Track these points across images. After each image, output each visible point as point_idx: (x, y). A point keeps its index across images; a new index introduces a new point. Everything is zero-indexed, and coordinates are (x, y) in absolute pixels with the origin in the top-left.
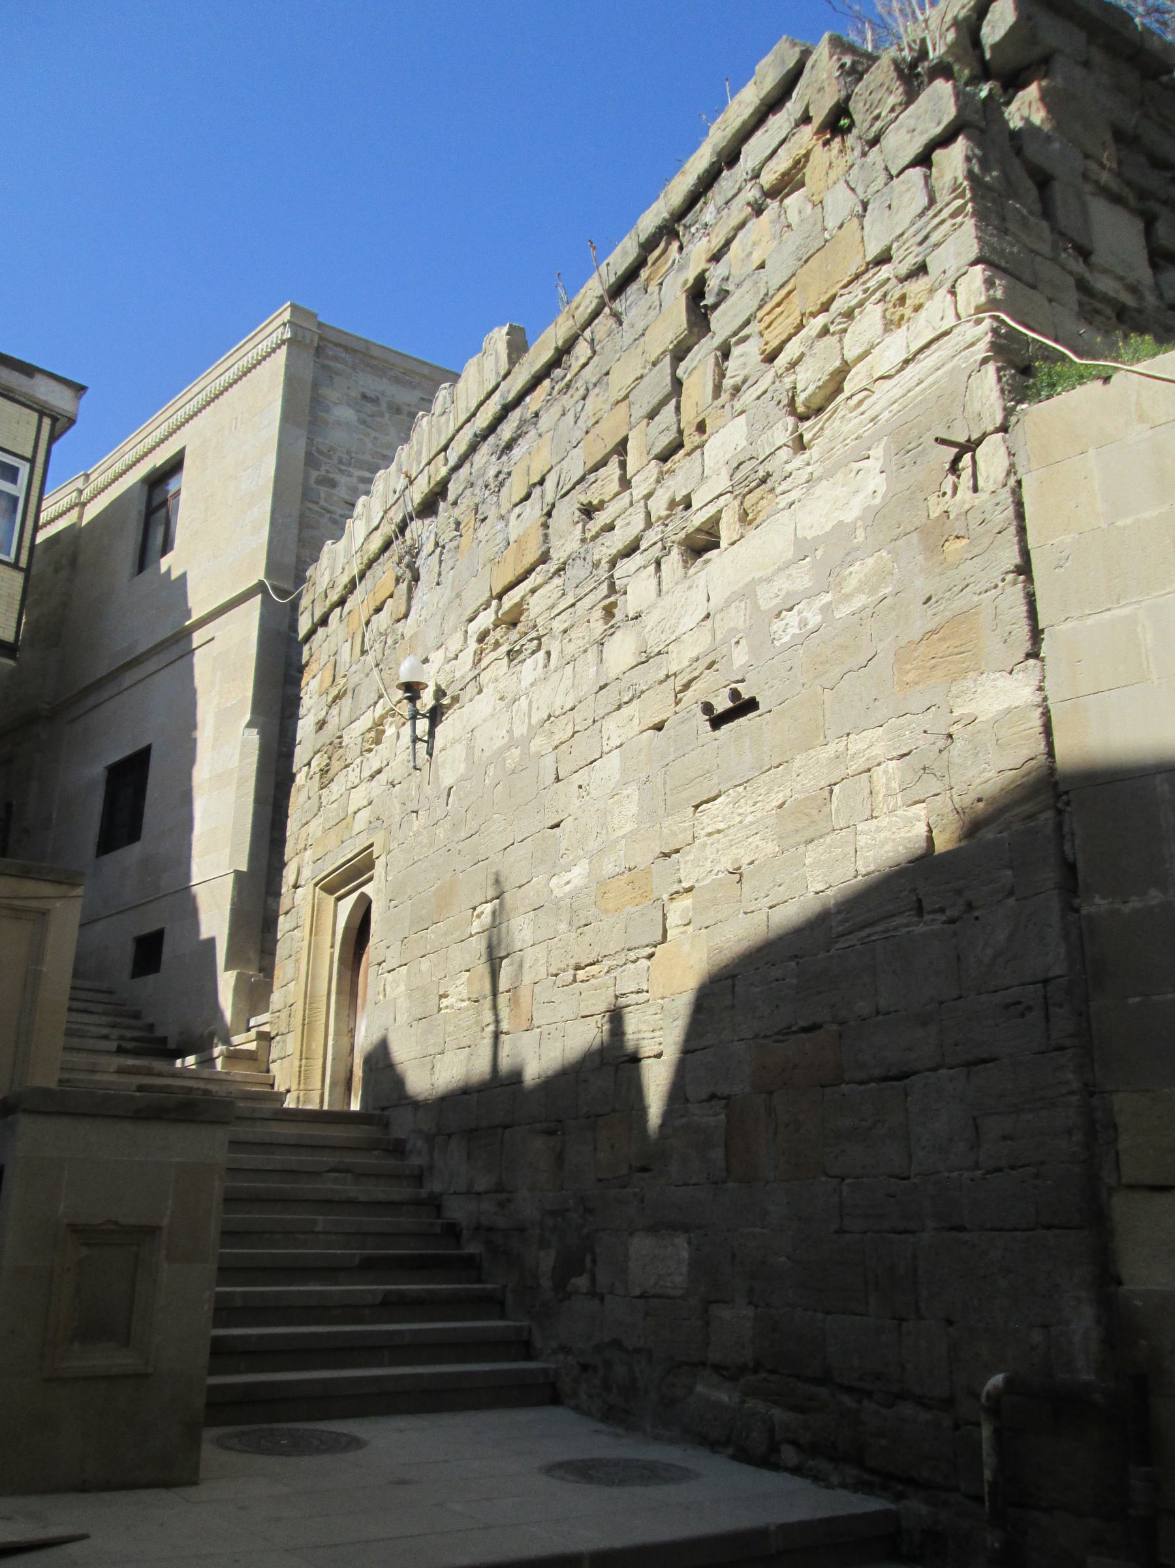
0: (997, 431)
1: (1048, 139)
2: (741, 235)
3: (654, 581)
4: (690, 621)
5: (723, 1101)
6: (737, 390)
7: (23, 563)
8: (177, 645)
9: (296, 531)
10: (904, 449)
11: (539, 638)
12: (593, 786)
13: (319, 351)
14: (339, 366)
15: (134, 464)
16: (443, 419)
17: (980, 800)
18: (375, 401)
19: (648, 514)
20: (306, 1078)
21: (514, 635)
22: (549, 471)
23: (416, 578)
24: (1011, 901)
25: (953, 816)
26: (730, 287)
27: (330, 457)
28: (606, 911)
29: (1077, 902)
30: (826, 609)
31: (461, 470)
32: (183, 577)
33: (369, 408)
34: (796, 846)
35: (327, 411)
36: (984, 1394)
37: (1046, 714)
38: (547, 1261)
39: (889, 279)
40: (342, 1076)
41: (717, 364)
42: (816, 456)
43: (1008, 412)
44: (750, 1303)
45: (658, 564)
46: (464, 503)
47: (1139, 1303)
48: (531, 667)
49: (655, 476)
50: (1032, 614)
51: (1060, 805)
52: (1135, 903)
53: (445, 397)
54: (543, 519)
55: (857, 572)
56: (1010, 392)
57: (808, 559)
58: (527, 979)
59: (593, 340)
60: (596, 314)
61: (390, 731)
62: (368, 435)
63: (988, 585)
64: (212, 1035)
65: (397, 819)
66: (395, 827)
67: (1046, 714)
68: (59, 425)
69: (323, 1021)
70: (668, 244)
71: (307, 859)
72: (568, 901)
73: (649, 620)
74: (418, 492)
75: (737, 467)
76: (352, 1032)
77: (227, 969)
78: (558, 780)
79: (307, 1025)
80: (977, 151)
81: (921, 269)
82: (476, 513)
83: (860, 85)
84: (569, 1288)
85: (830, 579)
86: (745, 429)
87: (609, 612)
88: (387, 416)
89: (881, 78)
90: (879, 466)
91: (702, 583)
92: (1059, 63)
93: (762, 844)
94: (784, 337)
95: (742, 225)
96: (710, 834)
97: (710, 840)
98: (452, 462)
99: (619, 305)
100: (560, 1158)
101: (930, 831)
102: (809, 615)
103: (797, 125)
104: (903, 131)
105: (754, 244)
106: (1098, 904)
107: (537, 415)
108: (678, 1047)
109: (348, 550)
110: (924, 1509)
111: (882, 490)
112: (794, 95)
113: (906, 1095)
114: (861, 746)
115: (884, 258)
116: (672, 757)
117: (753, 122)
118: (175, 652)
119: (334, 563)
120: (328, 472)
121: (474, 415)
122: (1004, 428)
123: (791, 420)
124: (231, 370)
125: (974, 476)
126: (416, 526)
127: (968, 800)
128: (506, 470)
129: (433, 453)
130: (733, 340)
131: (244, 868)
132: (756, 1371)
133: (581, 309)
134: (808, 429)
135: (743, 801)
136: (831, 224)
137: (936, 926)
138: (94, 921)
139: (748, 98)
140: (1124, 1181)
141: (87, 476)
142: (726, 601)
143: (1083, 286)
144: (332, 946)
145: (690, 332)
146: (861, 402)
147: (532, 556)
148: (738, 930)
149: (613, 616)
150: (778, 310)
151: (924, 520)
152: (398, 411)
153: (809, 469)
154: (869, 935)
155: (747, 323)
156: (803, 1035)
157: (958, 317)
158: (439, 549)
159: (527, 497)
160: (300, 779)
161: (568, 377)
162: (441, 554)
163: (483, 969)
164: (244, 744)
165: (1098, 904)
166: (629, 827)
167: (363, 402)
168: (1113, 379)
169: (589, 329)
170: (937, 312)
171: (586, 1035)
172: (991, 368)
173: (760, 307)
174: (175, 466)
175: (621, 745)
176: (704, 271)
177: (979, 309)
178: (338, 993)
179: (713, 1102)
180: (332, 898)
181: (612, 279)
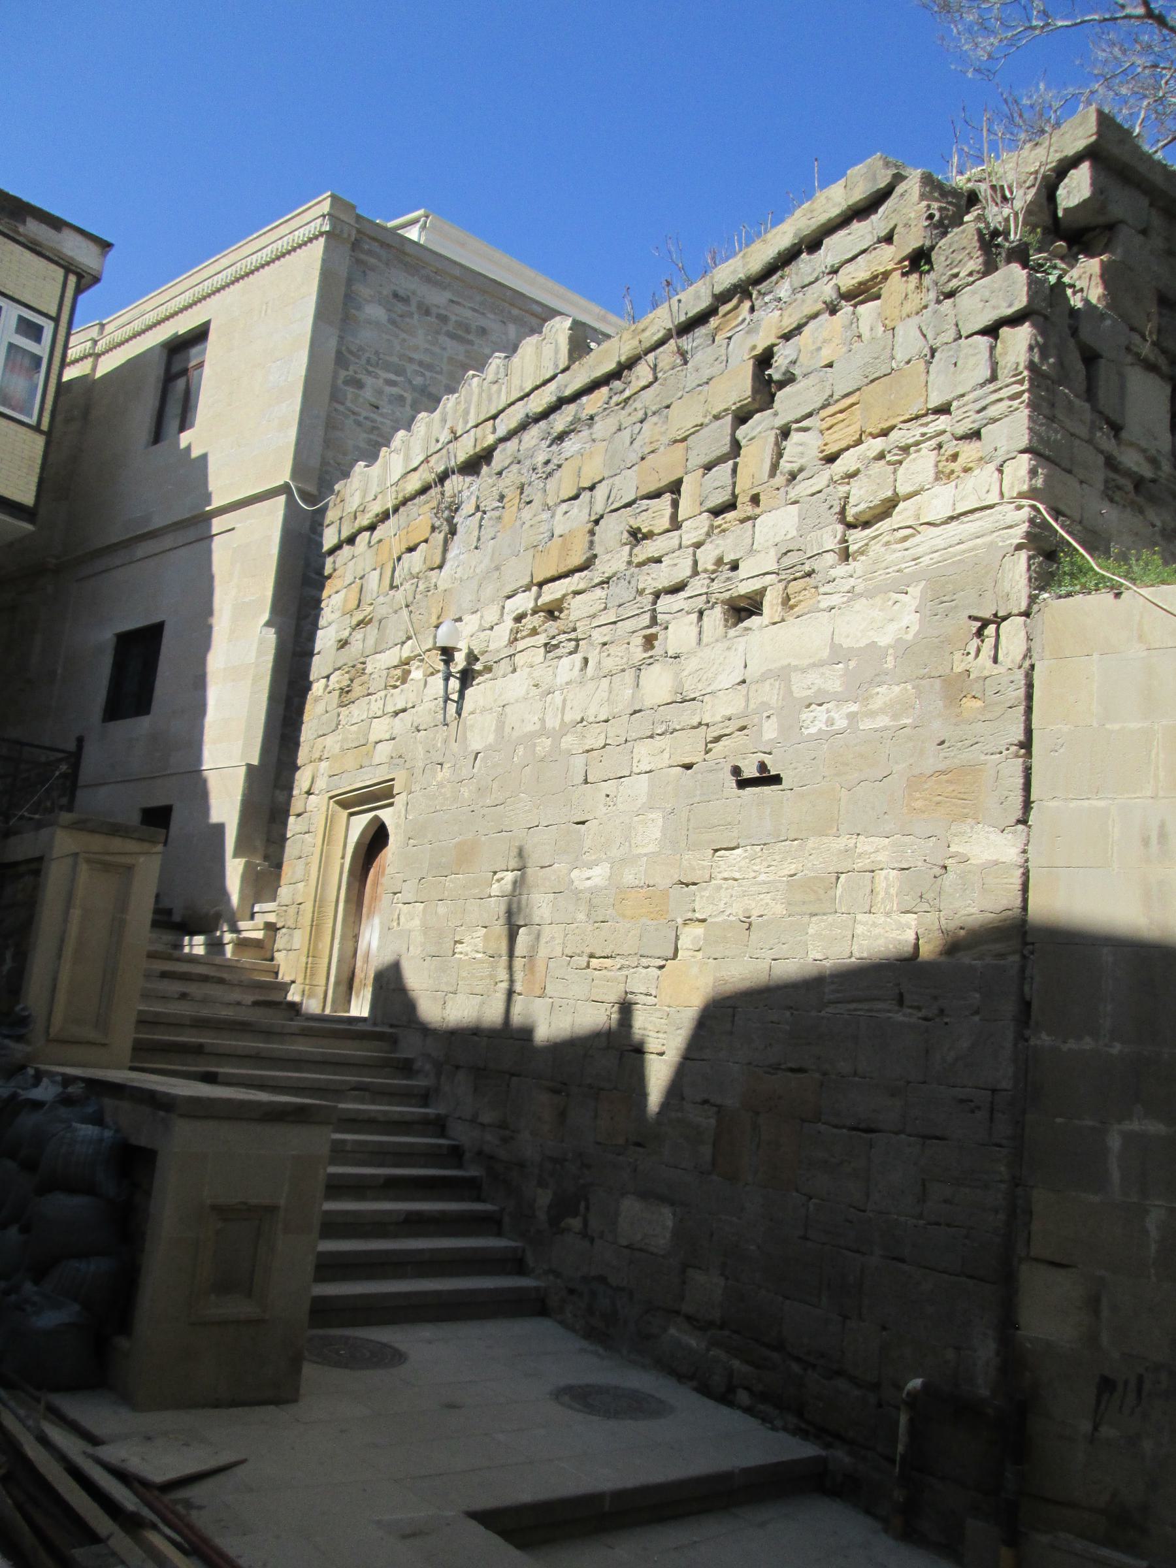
0: (1021, 614)
1: (1103, 316)
2: (812, 324)
3: (696, 630)
4: (727, 679)
5: (715, 1109)
6: (793, 476)
7: (45, 426)
8: (195, 527)
9: (321, 433)
10: (940, 594)
11: (577, 640)
12: (620, 800)
13: (355, 245)
14: (372, 261)
15: (154, 325)
16: (495, 387)
17: (962, 928)
18: (405, 300)
19: (695, 563)
20: (312, 975)
21: (552, 627)
22: (600, 482)
23: (453, 532)
24: (977, 1018)
25: (938, 934)
26: (796, 371)
27: (359, 357)
28: (624, 916)
29: (1027, 1033)
30: (852, 717)
31: (509, 443)
32: (204, 457)
33: (400, 307)
34: (803, 914)
35: (359, 308)
36: (905, 1392)
37: (1026, 875)
38: (544, 1198)
39: (945, 432)
40: (345, 976)
41: (777, 444)
42: (859, 573)
43: (1033, 599)
44: (722, 1274)
45: (701, 613)
46: (512, 477)
47: (1029, 1345)
48: (568, 667)
49: (705, 529)
51: (1026, 952)
52: (1072, 1044)
53: (498, 367)
54: (590, 525)
55: (884, 694)
56: (1036, 579)
57: (841, 665)
58: (543, 952)
59: (656, 366)
60: (662, 343)
61: (417, 674)
62: (397, 336)
63: (994, 749)
65: (421, 764)
67: (1026, 875)
68: (83, 281)
69: (331, 925)
70: (741, 301)
71: (322, 771)
72: (588, 895)
74: (464, 450)
75: (785, 554)
76: (356, 937)
77: (236, 855)
78: (586, 782)
79: (316, 927)
80: (1039, 339)
81: (976, 435)
82: (522, 493)
83: (943, 241)
84: (563, 1225)
86: (797, 519)
87: (649, 642)
88: (416, 316)
89: (965, 243)
90: (914, 604)
92: (1124, 232)
93: (772, 904)
94: (843, 445)
95: (815, 316)
96: (726, 879)
97: (725, 884)
98: (501, 431)
99: (686, 342)
100: (562, 1115)
101: (918, 939)
102: (836, 716)
103: (879, 241)
104: (977, 297)
105: (824, 341)
106: (1044, 1039)
107: (592, 418)
108: (680, 1052)
109: (382, 480)
110: (847, 1460)
111: (915, 628)
112: (881, 210)
113: (871, 1147)
116: (697, 799)
117: (839, 220)
118: (191, 534)
119: (365, 488)
120: (356, 372)
121: (528, 395)
122: (1027, 614)
123: (840, 528)
124: (264, 251)
125: (996, 647)
126: (455, 483)
127: (952, 925)
128: (556, 462)
129: (482, 418)
130: (795, 426)
131: (255, 762)
132: (721, 1328)
133: (647, 334)
134: (857, 537)
135: (758, 860)
136: (900, 355)
137: (913, 1020)
138: (101, 784)
139: (834, 199)
140: (1032, 1254)
141: (102, 326)
142: (763, 674)
143: (1111, 463)
144: (343, 857)
145: (754, 399)
146: (905, 539)
147: (577, 560)
148: (746, 968)
149: (652, 647)
150: (840, 416)
151: (948, 671)
153: (852, 582)
154: (855, 1010)
155: (810, 415)
156: (789, 1074)
157: (1002, 495)
158: (479, 514)
160: (317, 688)
161: (627, 394)
162: (482, 518)
163: (500, 929)
164: (261, 642)
165: (1044, 1039)
166: (652, 848)
167: (395, 301)
168: (1123, 596)
169: (653, 354)
170: (980, 485)
172: (1023, 555)
173: (823, 407)
174: (200, 335)
175: (650, 771)
176: (774, 345)
177: (1021, 495)
178: (347, 901)
179: (706, 1107)
181: (683, 318)
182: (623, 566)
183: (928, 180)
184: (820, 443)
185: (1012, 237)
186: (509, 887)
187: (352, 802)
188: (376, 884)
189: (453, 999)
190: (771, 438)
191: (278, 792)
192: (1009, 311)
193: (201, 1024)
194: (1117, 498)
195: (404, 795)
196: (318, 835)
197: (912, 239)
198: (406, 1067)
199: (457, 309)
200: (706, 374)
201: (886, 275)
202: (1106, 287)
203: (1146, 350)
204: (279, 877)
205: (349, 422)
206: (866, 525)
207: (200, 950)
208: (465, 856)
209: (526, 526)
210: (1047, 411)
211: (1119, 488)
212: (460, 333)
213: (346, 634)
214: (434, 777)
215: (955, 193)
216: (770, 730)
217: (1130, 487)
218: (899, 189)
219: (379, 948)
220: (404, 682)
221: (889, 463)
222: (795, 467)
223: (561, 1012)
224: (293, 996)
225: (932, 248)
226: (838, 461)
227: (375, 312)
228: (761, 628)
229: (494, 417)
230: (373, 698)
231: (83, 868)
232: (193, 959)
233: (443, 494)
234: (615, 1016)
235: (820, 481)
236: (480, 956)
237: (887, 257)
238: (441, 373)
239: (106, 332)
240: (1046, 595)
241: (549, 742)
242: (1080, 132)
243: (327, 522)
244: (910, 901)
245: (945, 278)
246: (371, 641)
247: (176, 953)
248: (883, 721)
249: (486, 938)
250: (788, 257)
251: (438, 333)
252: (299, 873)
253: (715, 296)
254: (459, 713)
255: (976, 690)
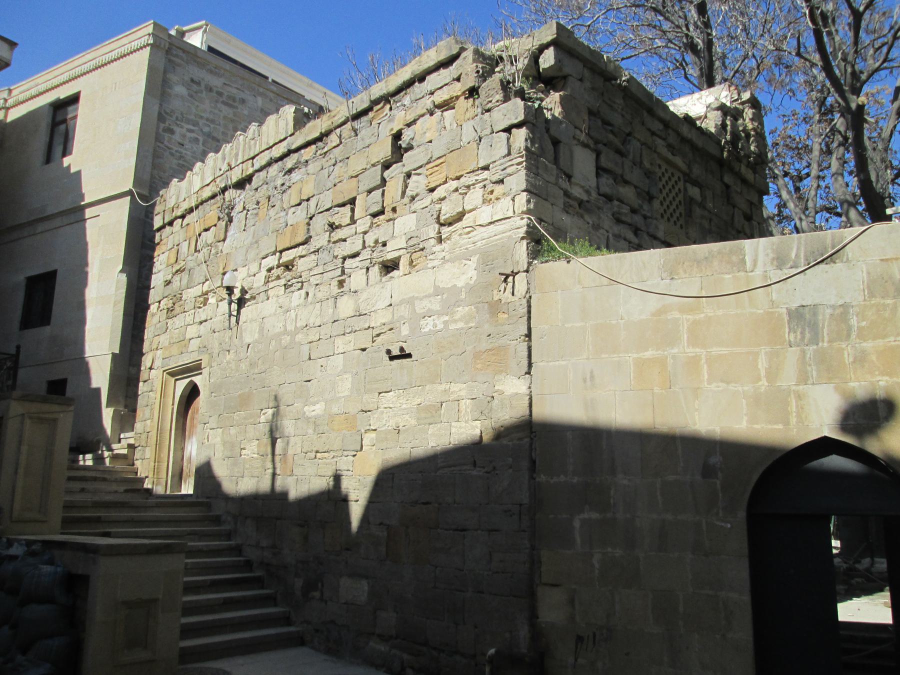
1: (561, 122)
2: (421, 119)
8: (76, 214)
9: (151, 160)
10: (486, 260)
11: (302, 282)
13: (168, 52)
14: (178, 61)
15: (44, 92)
16: (252, 142)
18: (198, 84)
19: (364, 242)
23: (231, 220)
24: (511, 471)
26: (414, 144)
27: (171, 116)
28: (333, 430)
29: (535, 475)
30: (445, 323)
35: (171, 88)
38: (299, 583)
40: (178, 472)
41: (404, 181)
43: (530, 264)
45: (368, 269)
46: (263, 191)
48: (297, 297)
50: (530, 356)
52: (555, 479)
54: (307, 220)
55: (461, 311)
58: (291, 452)
61: (212, 300)
64: (98, 442)
65: (217, 351)
66: (215, 355)
70: (385, 105)
71: (158, 355)
73: (363, 296)
76: (183, 449)
77: (107, 406)
78: (310, 359)
79: (158, 445)
81: (501, 181)
85: (448, 309)
87: (341, 283)
89: (494, 86)
91: (389, 287)
94: (438, 183)
95: (423, 115)
98: (257, 167)
99: (356, 124)
103: (454, 80)
104: (501, 113)
106: (542, 478)
107: (307, 162)
111: (475, 278)
114: (456, 389)
115: (486, 168)
119: (177, 194)
121: (271, 147)
122: (527, 271)
123: (437, 226)
126: (230, 194)
127: (497, 426)
129: (246, 158)
133: (336, 118)
134: (446, 230)
136: (465, 140)
139: (431, 57)
141: (10, 91)
143: (567, 194)
144: (173, 404)
146: (469, 233)
147: (300, 239)
148: (399, 452)
149: (343, 287)
150: (436, 169)
152: (211, 90)
153: (444, 254)
155: (421, 167)
158: (245, 212)
159: (299, 204)
160: (153, 308)
161: (326, 150)
163: (266, 440)
164: (118, 282)
165: (542, 478)
166: (347, 393)
170: (504, 207)
171: (319, 483)
172: (525, 242)
173: (428, 163)
174: (74, 99)
176: (402, 129)
177: (523, 213)
178: (176, 430)
180: (173, 379)
181: (355, 112)
182: (326, 243)
183: (477, 52)
184: (426, 182)
185: (516, 84)
186: (270, 417)
187: (176, 374)
188: (193, 419)
189: (242, 478)
190: (401, 177)
191: (131, 369)
192: (516, 121)
193: (97, 505)
194: (570, 211)
195: (207, 369)
196: (156, 393)
197: (470, 81)
198: (217, 520)
199: (229, 89)
200: (367, 143)
201: (457, 98)
202: (563, 108)
203: (583, 137)
204: (135, 417)
205: (167, 154)
206: (450, 224)
207: (90, 463)
208: (244, 401)
209: (272, 219)
210: (535, 171)
211: (571, 206)
212: (231, 102)
213: (170, 277)
214: (225, 358)
215: (491, 58)
216: (405, 331)
217: (576, 204)
218: (463, 55)
219: (197, 455)
220: (205, 305)
221: (460, 194)
222: (414, 193)
223: (303, 481)
224: (147, 485)
225: (479, 87)
226: (435, 192)
227: (180, 90)
228: (399, 277)
229: (253, 158)
230: (187, 314)
231: (28, 422)
232: (86, 468)
233: (224, 199)
234: (331, 483)
235: (427, 201)
236: (255, 456)
237: (458, 89)
238: (219, 125)
239: (13, 94)
240: (536, 262)
241: (289, 338)
242: (549, 32)
243: (156, 212)
244: (477, 415)
245: (485, 102)
246: (184, 282)
247: (75, 465)
248: (460, 325)
249: (259, 445)
250: (408, 85)
251: (217, 102)
252: (147, 414)
253: (371, 101)
254: (237, 322)
255: (504, 309)
